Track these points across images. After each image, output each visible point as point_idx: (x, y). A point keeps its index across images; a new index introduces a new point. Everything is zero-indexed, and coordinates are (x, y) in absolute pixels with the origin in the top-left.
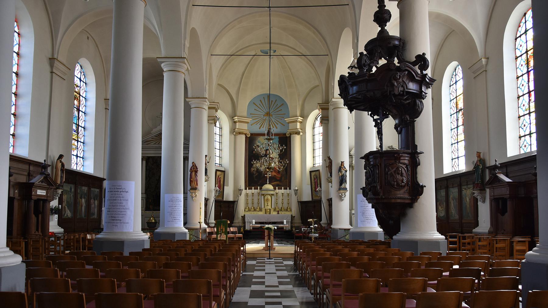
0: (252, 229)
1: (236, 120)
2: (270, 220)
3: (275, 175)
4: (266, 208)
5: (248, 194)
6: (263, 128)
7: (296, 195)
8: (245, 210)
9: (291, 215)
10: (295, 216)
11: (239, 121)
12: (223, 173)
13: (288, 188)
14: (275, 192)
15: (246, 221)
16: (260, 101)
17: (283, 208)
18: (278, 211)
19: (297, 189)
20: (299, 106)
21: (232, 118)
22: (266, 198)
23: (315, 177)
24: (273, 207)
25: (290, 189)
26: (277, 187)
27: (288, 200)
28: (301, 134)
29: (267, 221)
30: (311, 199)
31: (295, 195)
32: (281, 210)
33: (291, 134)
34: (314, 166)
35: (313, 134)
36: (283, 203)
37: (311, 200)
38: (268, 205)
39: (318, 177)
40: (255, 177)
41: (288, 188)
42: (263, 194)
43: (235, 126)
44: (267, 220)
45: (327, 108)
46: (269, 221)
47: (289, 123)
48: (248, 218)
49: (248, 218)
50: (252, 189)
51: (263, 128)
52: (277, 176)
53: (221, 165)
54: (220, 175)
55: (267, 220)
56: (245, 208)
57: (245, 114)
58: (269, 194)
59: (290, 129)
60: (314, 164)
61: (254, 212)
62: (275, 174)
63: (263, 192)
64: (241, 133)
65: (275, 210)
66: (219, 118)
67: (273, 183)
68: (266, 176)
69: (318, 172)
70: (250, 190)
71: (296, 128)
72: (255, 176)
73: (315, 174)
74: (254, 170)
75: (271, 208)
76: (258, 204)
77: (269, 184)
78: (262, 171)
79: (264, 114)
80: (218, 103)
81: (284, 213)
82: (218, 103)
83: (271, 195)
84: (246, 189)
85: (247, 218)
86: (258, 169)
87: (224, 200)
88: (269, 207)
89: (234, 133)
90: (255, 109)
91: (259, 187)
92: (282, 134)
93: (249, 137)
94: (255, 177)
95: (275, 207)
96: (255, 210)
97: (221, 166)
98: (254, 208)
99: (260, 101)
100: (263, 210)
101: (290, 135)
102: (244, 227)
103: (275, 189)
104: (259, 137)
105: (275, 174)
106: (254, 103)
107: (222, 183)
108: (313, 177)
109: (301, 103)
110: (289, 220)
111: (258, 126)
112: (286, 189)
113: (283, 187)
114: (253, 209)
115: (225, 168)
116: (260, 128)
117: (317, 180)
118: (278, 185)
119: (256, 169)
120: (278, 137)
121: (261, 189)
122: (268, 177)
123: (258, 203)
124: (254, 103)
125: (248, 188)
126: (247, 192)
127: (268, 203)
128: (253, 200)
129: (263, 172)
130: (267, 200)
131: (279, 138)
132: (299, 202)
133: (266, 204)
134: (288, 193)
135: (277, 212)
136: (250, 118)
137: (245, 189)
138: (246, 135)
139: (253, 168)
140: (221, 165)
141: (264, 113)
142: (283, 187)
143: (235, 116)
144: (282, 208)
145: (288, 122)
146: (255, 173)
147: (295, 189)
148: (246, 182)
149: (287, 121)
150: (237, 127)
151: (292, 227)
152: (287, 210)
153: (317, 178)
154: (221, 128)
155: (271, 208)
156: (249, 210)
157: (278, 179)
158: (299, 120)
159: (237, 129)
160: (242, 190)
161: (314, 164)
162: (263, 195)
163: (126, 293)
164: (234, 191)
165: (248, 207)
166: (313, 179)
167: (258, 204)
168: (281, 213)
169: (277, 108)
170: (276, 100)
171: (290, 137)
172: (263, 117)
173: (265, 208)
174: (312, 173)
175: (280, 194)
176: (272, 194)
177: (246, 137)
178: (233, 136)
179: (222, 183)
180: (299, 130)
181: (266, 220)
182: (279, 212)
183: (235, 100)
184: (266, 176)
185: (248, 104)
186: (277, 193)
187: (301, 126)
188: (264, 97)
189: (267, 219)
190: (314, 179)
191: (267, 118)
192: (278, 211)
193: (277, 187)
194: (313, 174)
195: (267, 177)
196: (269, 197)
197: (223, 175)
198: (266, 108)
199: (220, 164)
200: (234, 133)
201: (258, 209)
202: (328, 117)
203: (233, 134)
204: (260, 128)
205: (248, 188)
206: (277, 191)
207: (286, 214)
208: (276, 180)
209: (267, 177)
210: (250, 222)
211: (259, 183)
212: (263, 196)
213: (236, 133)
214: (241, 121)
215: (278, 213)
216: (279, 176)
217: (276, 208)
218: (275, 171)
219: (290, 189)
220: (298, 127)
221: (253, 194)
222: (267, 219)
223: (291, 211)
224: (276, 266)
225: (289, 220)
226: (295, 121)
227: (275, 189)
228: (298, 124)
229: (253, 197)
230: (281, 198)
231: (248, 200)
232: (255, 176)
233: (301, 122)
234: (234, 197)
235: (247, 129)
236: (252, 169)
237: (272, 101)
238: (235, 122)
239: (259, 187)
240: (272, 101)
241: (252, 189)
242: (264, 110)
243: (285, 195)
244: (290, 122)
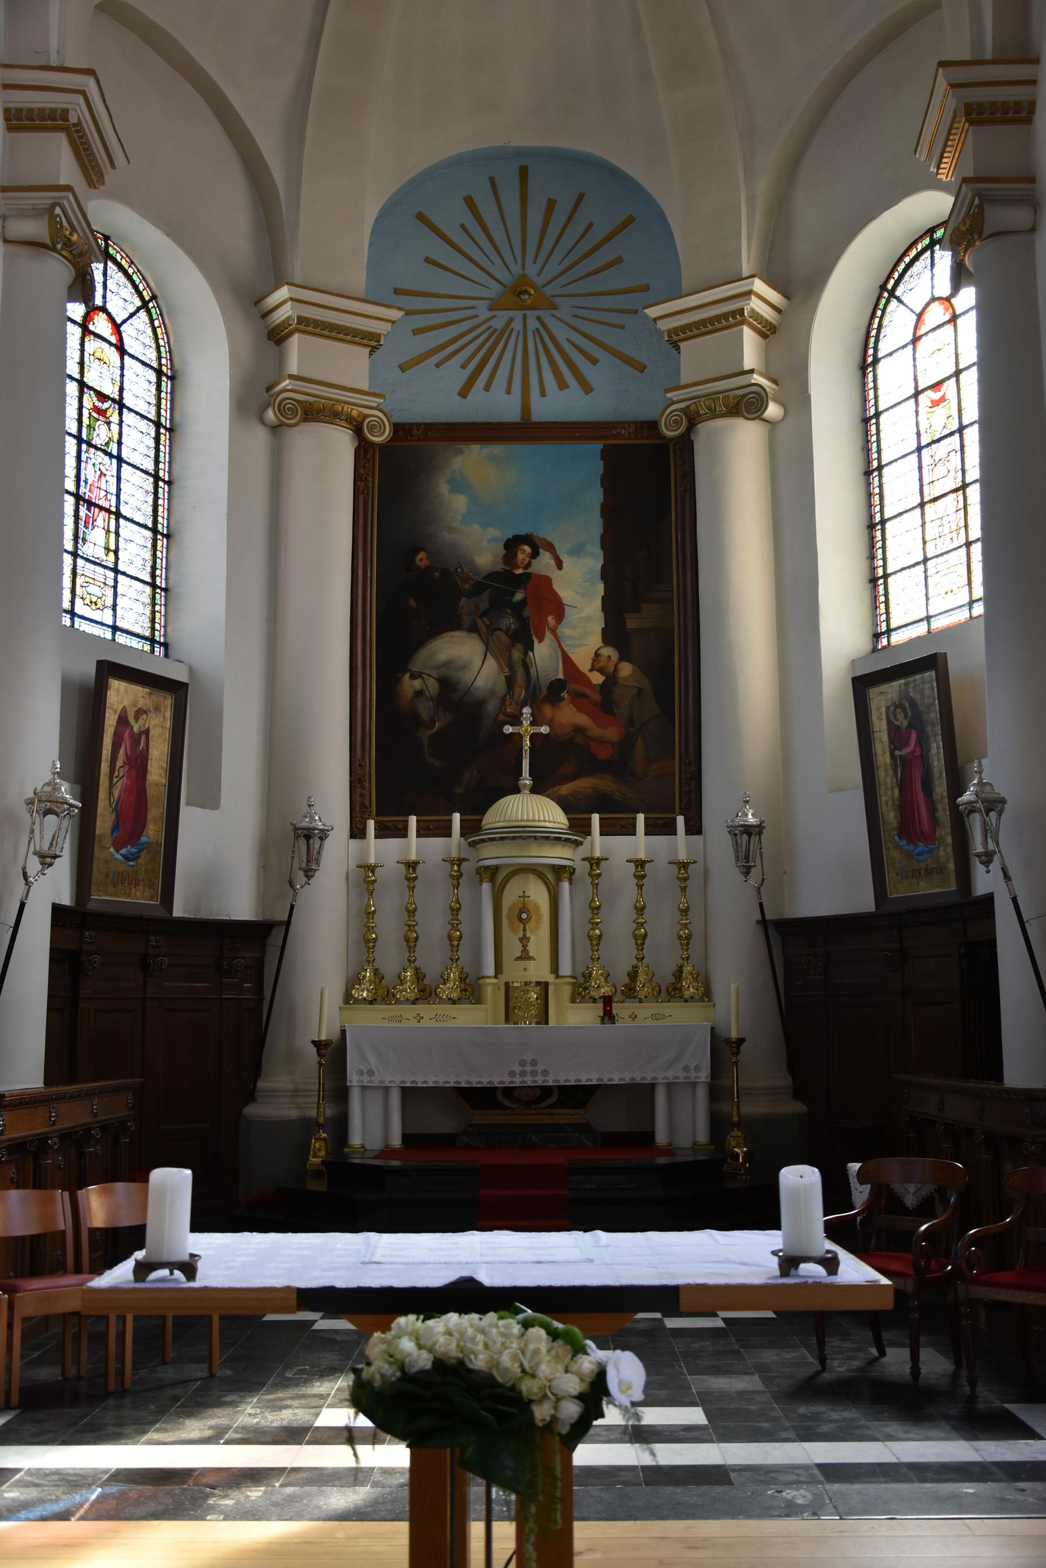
0: (396, 1141)
1: (286, 312)
2: (545, 1073)
3: (579, 730)
4: (517, 973)
5: (372, 869)
6: (487, 388)
7: (747, 871)
8: (348, 998)
9: (712, 1029)
10: (741, 1041)
11: (301, 320)
12: (167, 702)
13: (680, 820)
14: (582, 851)
15: (353, 1078)
16: (469, 201)
17: (642, 978)
18: (607, 1001)
19: (751, 819)
20: (751, 212)
21: (256, 303)
22: (511, 895)
23: (902, 722)
24: (566, 969)
25: (695, 828)
26: (596, 818)
27: (685, 912)
28: (773, 410)
29: (517, 1081)
30: (864, 902)
31: (736, 874)
32: (630, 992)
33: (693, 419)
34: (875, 650)
35: (865, 409)
36: (641, 941)
37: (873, 910)
38: (525, 956)
39: (934, 715)
40: (425, 742)
41: (680, 820)
42: (487, 868)
43: (281, 360)
44: (534, 1073)
45: (1018, 106)
46: (540, 1080)
47: (675, 339)
48: (372, 1059)
49: (372, 1059)
50: (403, 833)
51: (487, 388)
52: (596, 731)
53: (165, 645)
54: (139, 713)
55: (534, 1073)
56: (353, 981)
57: (357, 279)
58: (536, 871)
59: (683, 382)
60: (877, 636)
61: (421, 1008)
62: (582, 719)
63: (492, 855)
64: (318, 412)
65: (580, 991)
66: (154, 297)
67: (565, 789)
68: (508, 729)
69: (931, 675)
70: (392, 844)
71: (738, 370)
72: (425, 734)
73: (905, 695)
74: (419, 694)
75: (550, 978)
76: (455, 949)
77: (534, 790)
78: (481, 703)
79: (492, 294)
80: (90, 72)
81: (655, 1017)
82: (90, 72)
83: (550, 877)
84: (357, 832)
85: (364, 1059)
86: (447, 684)
87: (178, 912)
88: (539, 969)
89: (270, 415)
90: (428, 260)
91: (457, 817)
92: (630, 423)
93: (382, 446)
94: (425, 742)
95: (581, 968)
96: (426, 994)
97: (166, 655)
98: (419, 976)
99: (469, 201)
100: (492, 989)
101: (692, 424)
102: (341, 1125)
103: (580, 827)
104: (462, 452)
105: (582, 719)
106: (421, 217)
107: (156, 773)
108: (880, 727)
109: (763, 186)
110: (697, 1069)
111: (455, 375)
112: (661, 827)
113: (641, 818)
114: (409, 990)
115: (191, 671)
116: (464, 393)
117: (923, 743)
118: (602, 803)
119: (433, 687)
120: (598, 447)
121: (470, 828)
122: (527, 742)
123: (453, 942)
124: (421, 217)
125: (371, 824)
126: (365, 853)
127: (524, 940)
128: (411, 913)
129: (491, 707)
130: (523, 913)
131: (607, 454)
132: (772, 931)
133: (512, 946)
134: (682, 857)
135: (598, 1009)
136: (389, 306)
137: (353, 836)
138: (358, 431)
139: (413, 677)
140: (165, 645)
141: (496, 289)
142: (641, 818)
143: (278, 286)
144: (633, 975)
145: (675, 331)
146: (425, 709)
147: (739, 821)
148: (360, 781)
149: (664, 325)
150: (293, 367)
151: (718, 1125)
152: (673, 992)
153: (917, 722)
154: (172, 378)
155: (550, 978)
156: (383, 996)
157: (603, 754)
158: (755, 304)
159: (291, 377)
160: (323, 835)
161: (877, 636)
162: (492, 880)
163: (326, 1179)
164: (266, 849)
165: (376, 972)
166: (880, 727)
167: (455, 949)
168: (633, 1017)
169: (585, 246)
170: (581, 196)
171: (685, 445)
172: (485, 314)
173: (503, 979)
174: (873, 692)
175: (619, 869)
176: (559, 871)
177: (364, 450)
178: (260, 437)
179: (156, 773)
180: (757, 379)
181: (512, 1074)
182: (617, 1009)
183: (278, 173)
184: (508, 729)
185: (370, 230)
186: (594, 862)
187: (767, 356)
188: (492, 180)
189: (523, 1063)
190: (897, 737)
191: (517, 325)
192: (607, 1001)
193: (596, 818)
194: (881, 698)
195: (520, 737)
196: (538, 894)
197: (168, 714)
198: (506, 253)
199: (152, 641)
200: (270, 415)
201: (450, 989)
202: (1032, 180)
203: (263, 422)
204: (464, 393)
205: (371, 824)
206: (598, 843)
207: (667, 1022)
208: (591, 766)
209: (520, 737)
210: (386, 1090)
211: (459, 790)
212: (486, 887)
213: (281, 410)
214: (317, 323)
215: (608, 1016)
216: (612, 733)
217: (588, 976)
218: (583, 695)
219: (695, 828)
220: (750, 360)
221: (412, 865)
222: (523, 1063)
223: (707, 994)
224: (496, 330)
225: (697, 1069)
226: (725, 316)
227: (580, 827)
228: (749, 336)
229: (412, 889)
230: (628, 896)
231: (370, 915)
232: (425, 734)
233: (767, 331)
234: (263, 894)
235: (364, 385)
236: (409, 685)
237: (551, 204)
238: (277, 336)
239: (457, 817)
240: (551, 204)
241: (403, 833)
242: (498, 270)
243: (661, 871)
244: (684, 328)
